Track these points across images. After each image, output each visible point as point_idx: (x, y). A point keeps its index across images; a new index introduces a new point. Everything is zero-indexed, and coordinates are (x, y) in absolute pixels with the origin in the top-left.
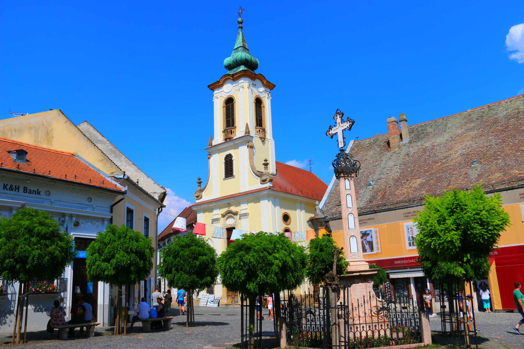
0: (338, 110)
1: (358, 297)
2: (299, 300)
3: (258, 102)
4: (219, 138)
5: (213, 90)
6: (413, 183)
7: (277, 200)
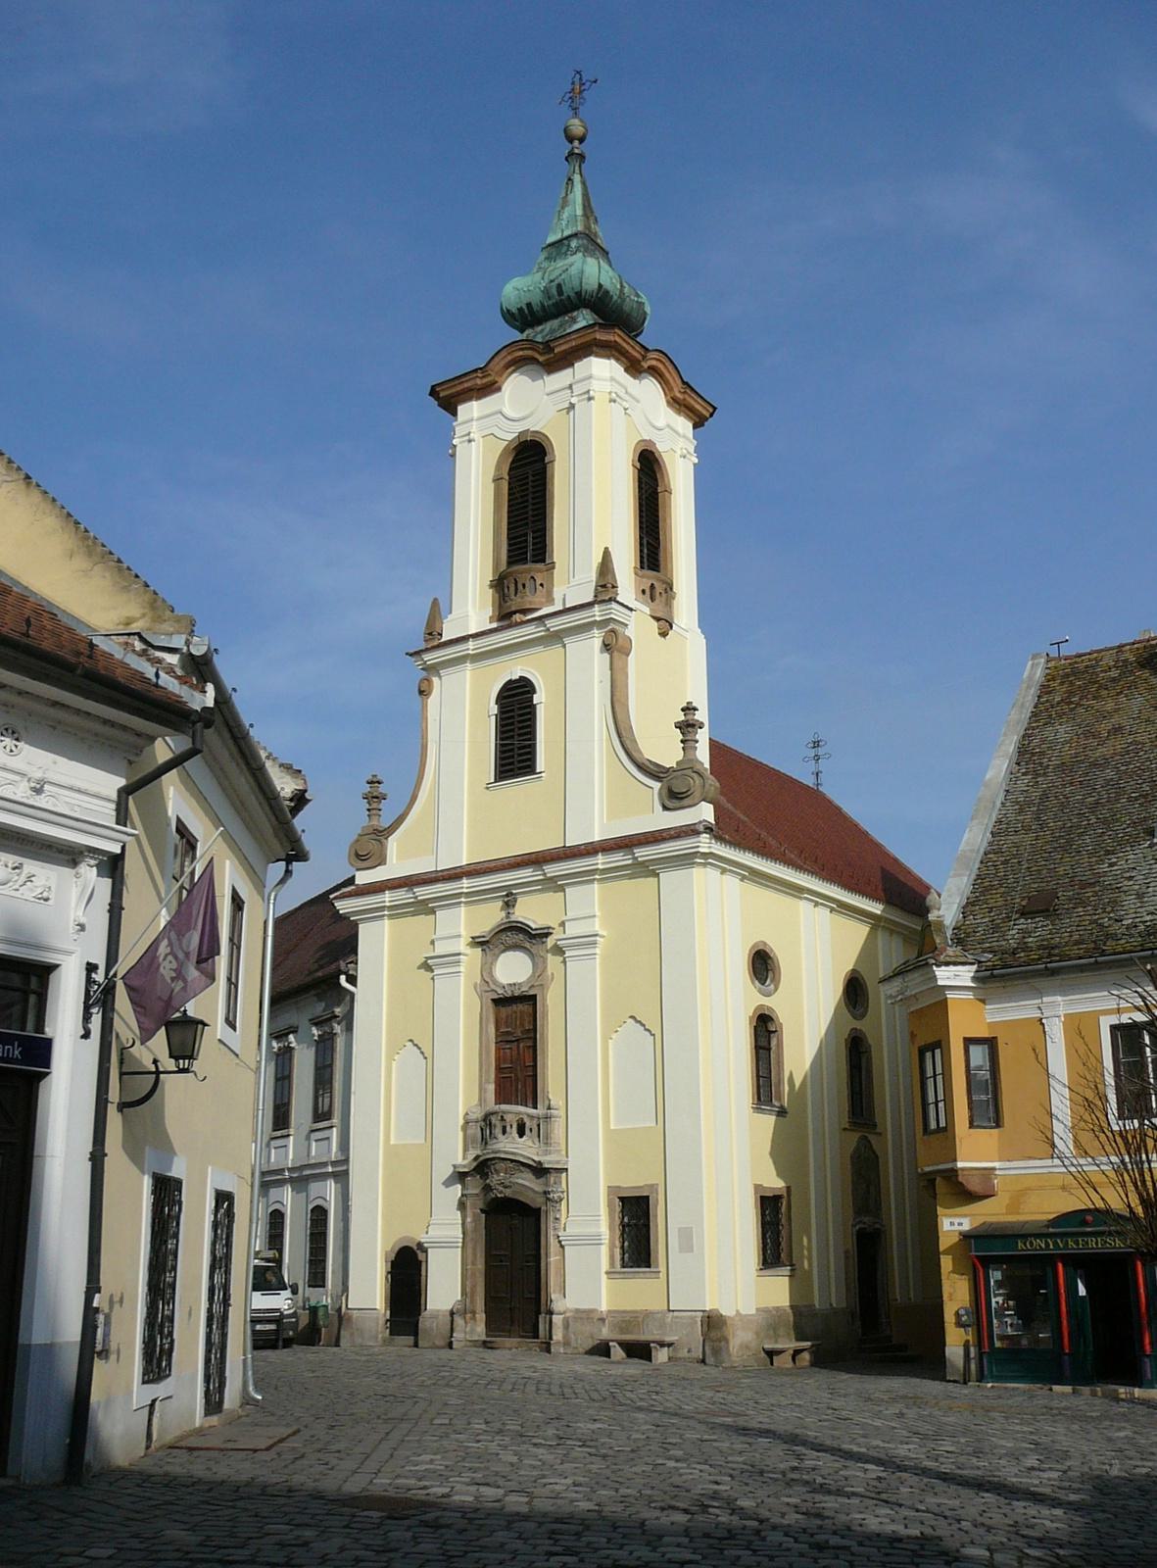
3: (648, 466)
4: (471, 608)
5: (450, 405)
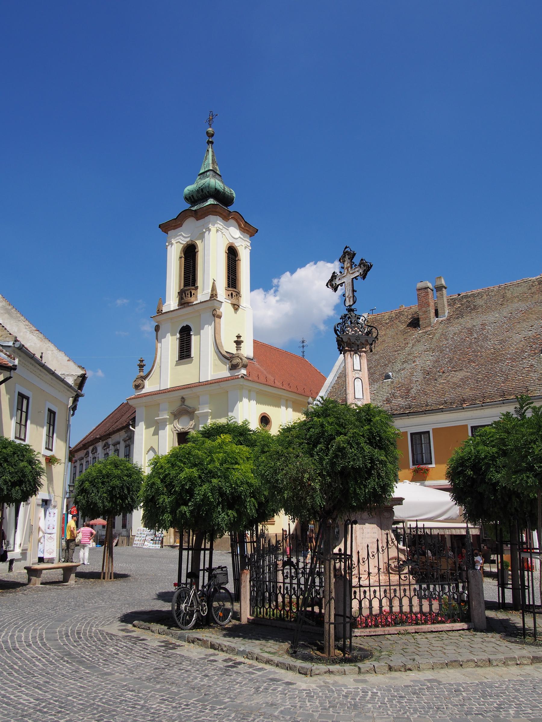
0: (346, 247)
1: (368, 541)
2: (274, 542)
3: (232, 253)
4: (172, 302)
6: (452, 377)
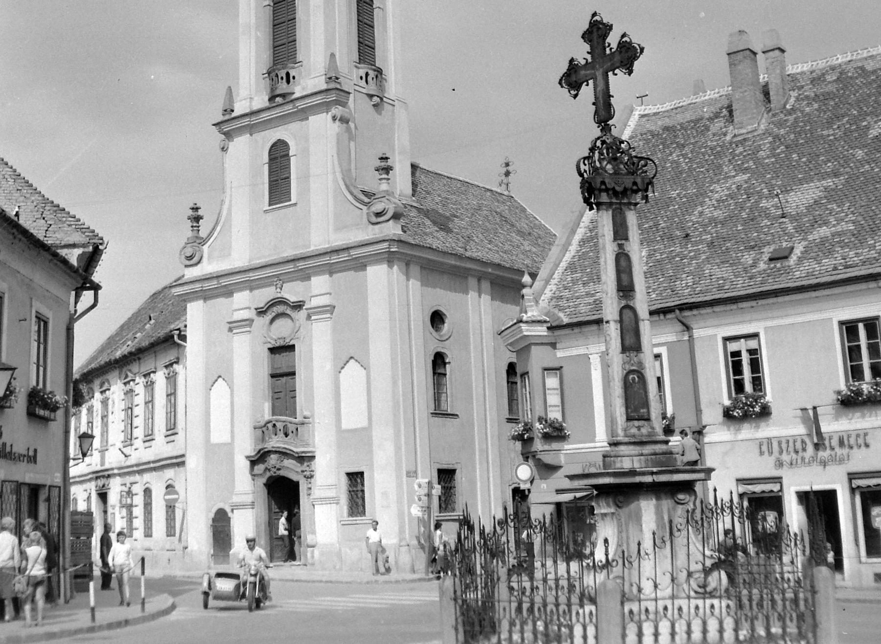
4: (251, 95)
7: (415, 269)
